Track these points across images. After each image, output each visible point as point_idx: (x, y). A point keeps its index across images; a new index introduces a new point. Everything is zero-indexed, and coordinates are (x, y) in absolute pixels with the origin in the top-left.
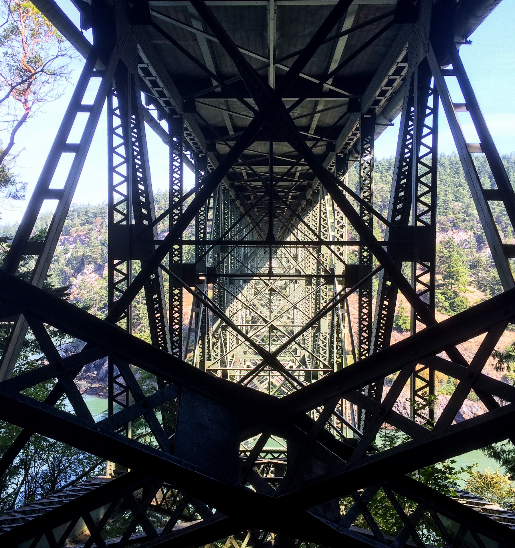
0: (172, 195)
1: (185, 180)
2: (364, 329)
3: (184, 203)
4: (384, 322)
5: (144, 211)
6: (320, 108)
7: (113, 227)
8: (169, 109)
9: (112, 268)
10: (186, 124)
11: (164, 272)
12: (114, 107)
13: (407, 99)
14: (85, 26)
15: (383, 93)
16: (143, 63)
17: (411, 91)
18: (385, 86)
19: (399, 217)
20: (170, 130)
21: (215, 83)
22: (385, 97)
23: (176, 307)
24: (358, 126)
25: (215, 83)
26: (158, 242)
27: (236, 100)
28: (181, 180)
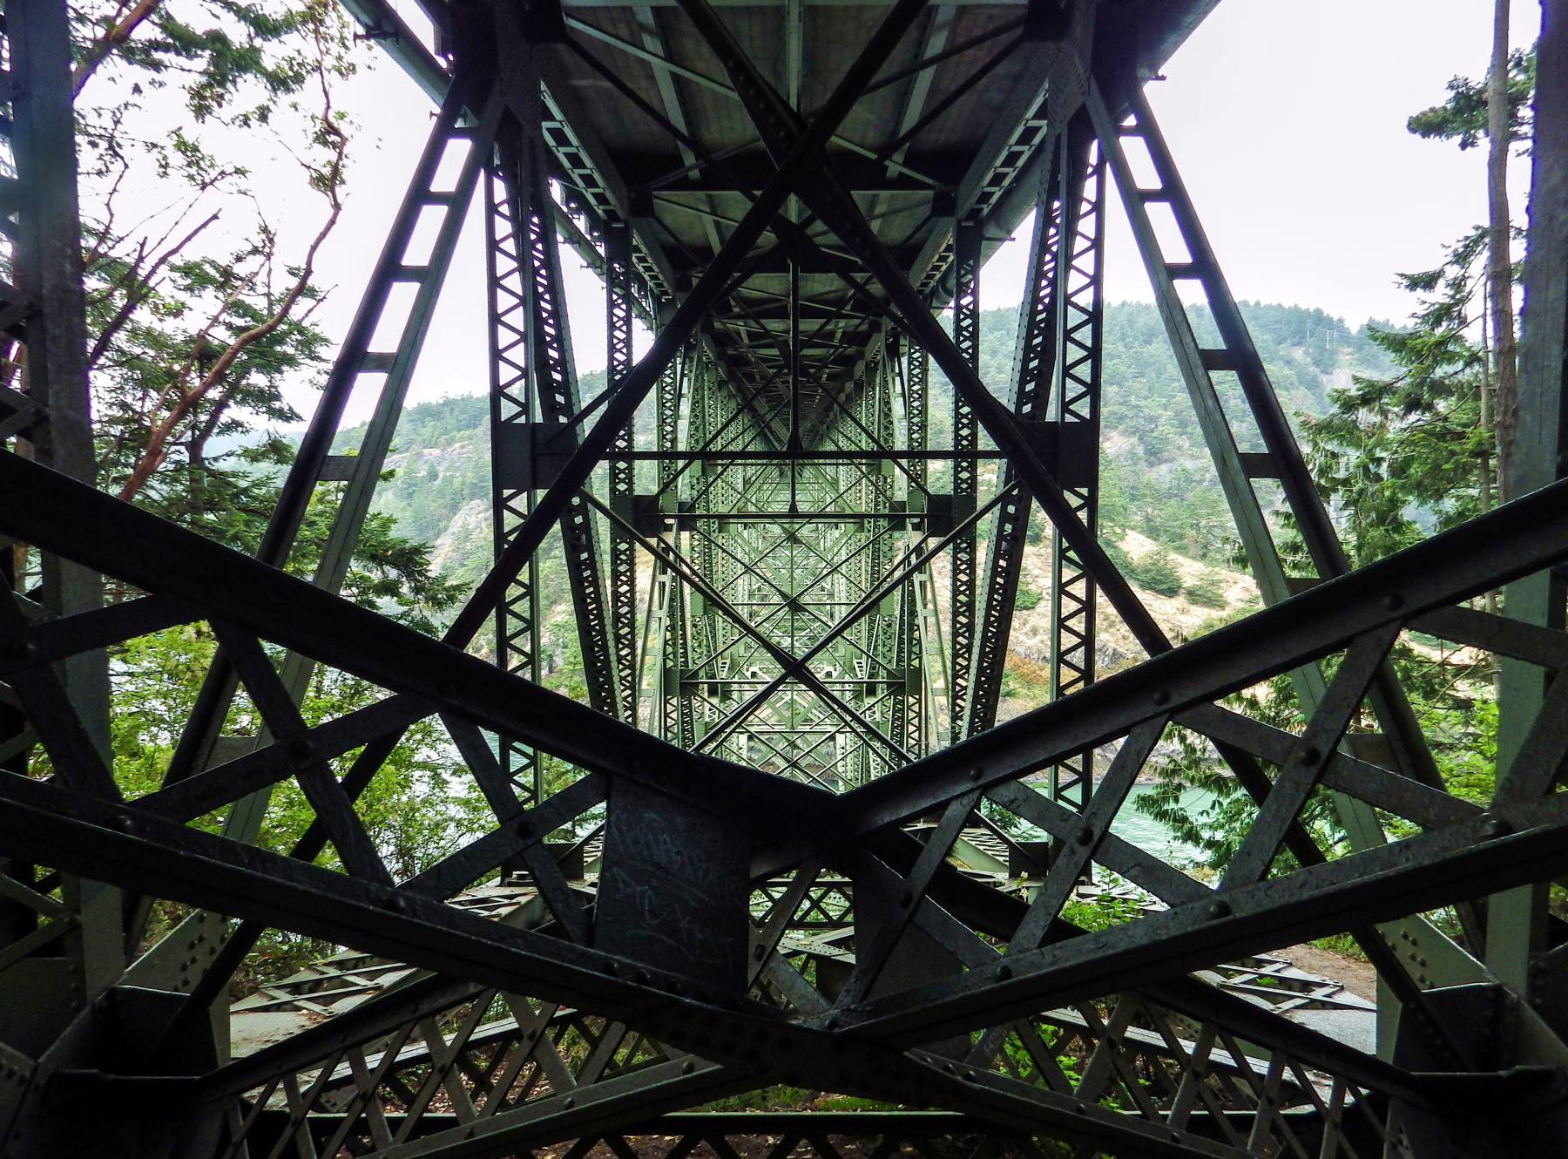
1: (635, 342)
5: (560, 399)
7: (500, 430)
10: (636, 240)
11: (599, 515)
13: (1046, 186)
15: (997, 180)
17: (1055, 172)
19: (1027, 409)
23: (624, 574)
28: (628, 342)
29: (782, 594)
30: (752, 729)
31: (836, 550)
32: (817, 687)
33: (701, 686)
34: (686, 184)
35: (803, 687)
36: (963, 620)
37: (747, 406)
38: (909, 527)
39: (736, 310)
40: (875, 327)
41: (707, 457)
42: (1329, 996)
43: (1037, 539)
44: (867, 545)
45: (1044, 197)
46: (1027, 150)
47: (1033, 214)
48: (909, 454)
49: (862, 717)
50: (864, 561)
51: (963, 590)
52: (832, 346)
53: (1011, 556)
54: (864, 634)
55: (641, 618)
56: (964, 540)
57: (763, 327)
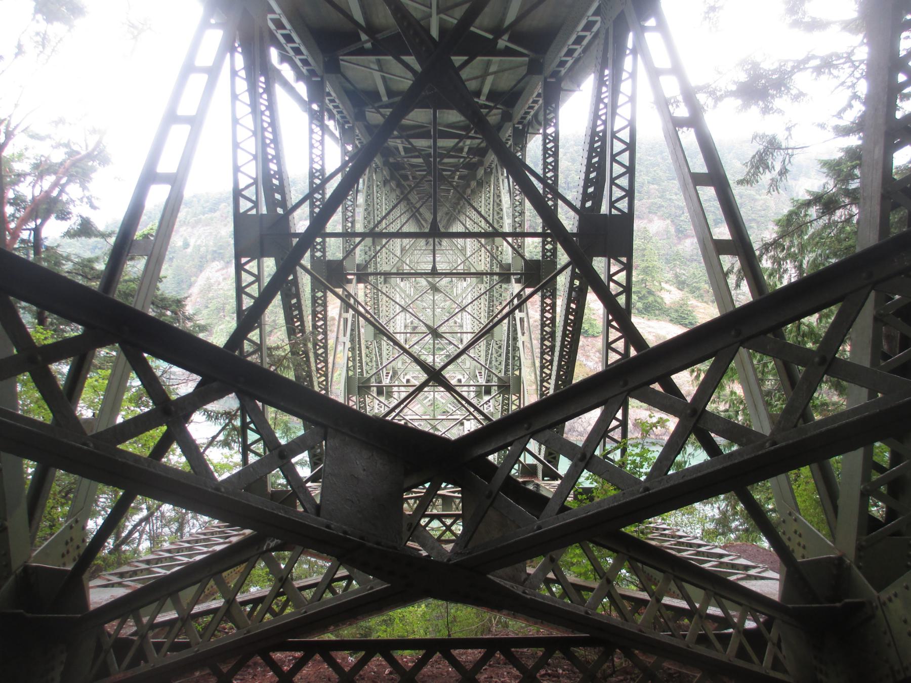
0: (312, 176)
3: (328, 186)
4: (571, 329)
6: (493, 69)
7: (240, 219)
9: (239, 268)
10: (328, 88)
16: (273, 12)
19: (589, 204)
21: (364, 37)
24: (540, 91)
25: (364, 37)
26: (296, 235)
27: (390, 58)
29: (426, 325)
31: (464, 296)
32: (449, 388)
33: (372, 388)
34: (362, 52)
35: (442, 389)
36: (547, 343)
37: (404, 198)
38: (513, 281)
41: (375, 235)
42: (759, 573)
44: (485, 293)
45: (599, 67)
46: (589, 36)
48: (514, 235)
49: (481, 409)
50: (484, 302)
51: (548, 324)
53: (578, 302)
54: (483, 354)
55: (331, 342)
56: (548, 289)
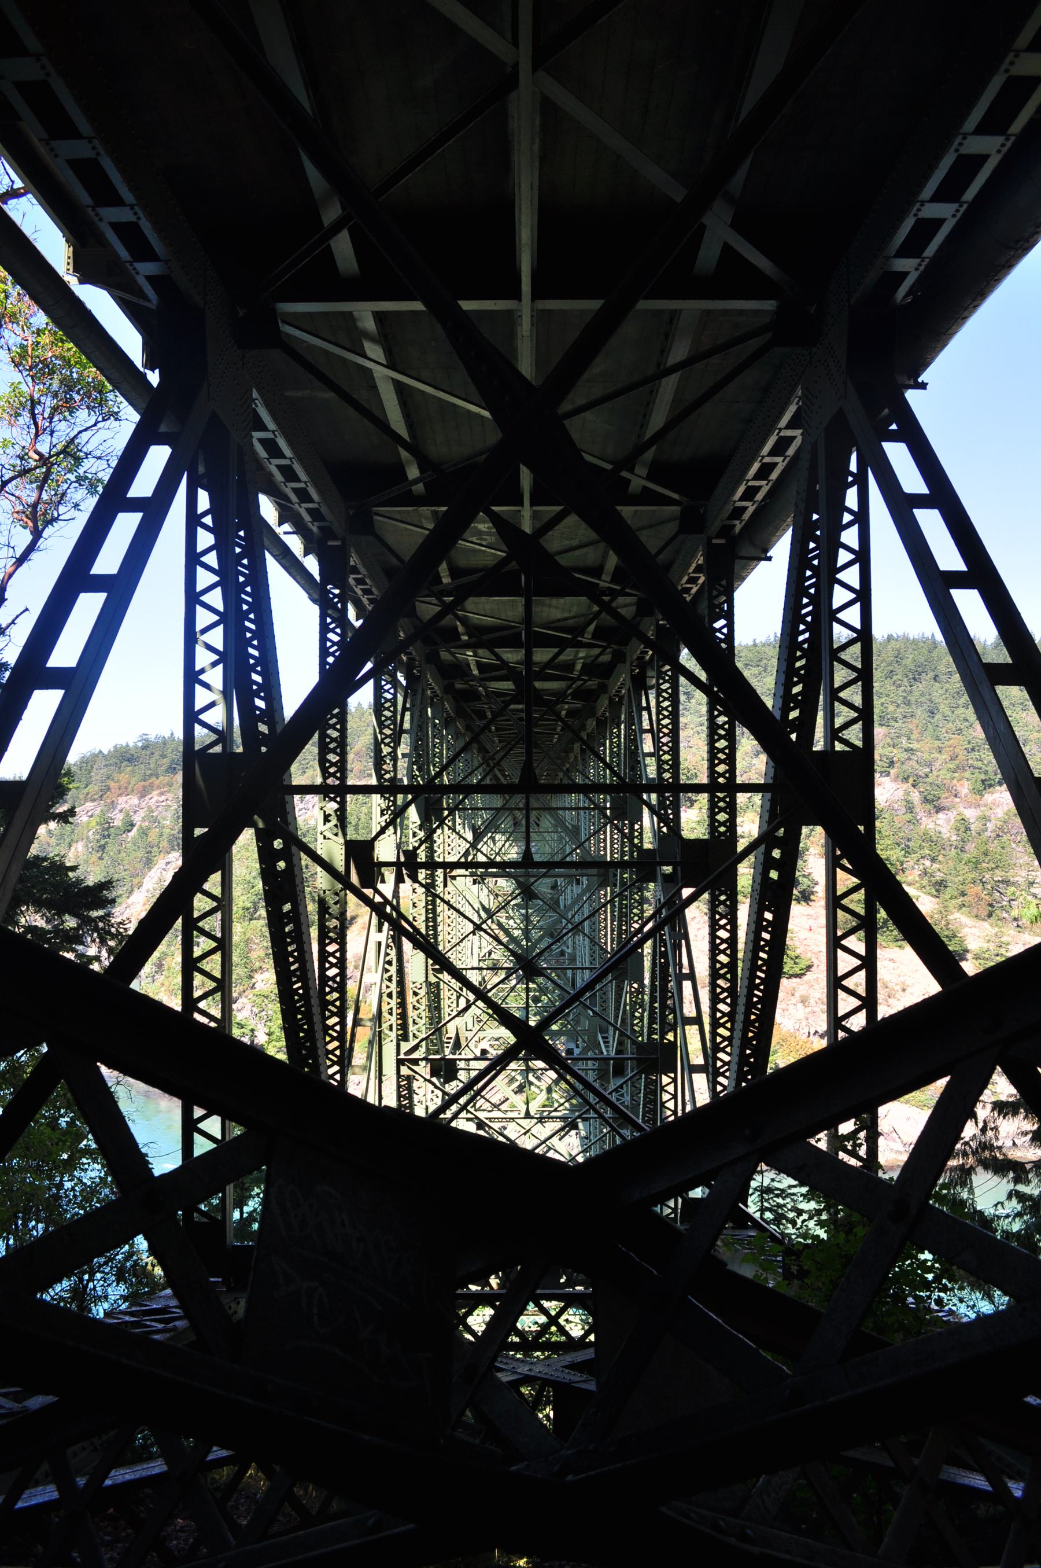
2: (722, 972)
8: (319, 527)
12: (200, 510)
14: (150, 365)
16: (265, 428)
17: (813, 480)
18: (770, 454)
20: (322, 573)
22: (755, 502)
24: (700, 562)
30: (482, 1115)
31: (576, 908)
39: (465, 638)
40: (619, 658)
43: (806, 897)
46: (781, 462)
47: (789, 532)
52: (571, 679)
57: (498, 657)
